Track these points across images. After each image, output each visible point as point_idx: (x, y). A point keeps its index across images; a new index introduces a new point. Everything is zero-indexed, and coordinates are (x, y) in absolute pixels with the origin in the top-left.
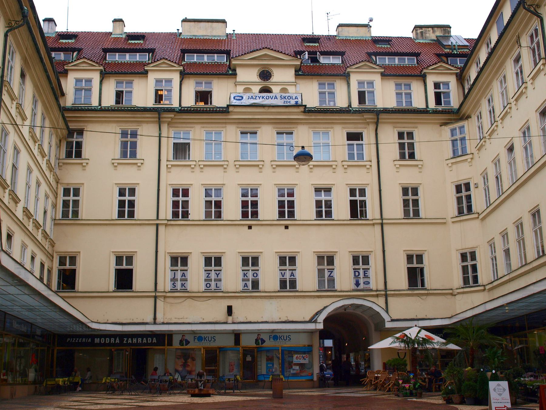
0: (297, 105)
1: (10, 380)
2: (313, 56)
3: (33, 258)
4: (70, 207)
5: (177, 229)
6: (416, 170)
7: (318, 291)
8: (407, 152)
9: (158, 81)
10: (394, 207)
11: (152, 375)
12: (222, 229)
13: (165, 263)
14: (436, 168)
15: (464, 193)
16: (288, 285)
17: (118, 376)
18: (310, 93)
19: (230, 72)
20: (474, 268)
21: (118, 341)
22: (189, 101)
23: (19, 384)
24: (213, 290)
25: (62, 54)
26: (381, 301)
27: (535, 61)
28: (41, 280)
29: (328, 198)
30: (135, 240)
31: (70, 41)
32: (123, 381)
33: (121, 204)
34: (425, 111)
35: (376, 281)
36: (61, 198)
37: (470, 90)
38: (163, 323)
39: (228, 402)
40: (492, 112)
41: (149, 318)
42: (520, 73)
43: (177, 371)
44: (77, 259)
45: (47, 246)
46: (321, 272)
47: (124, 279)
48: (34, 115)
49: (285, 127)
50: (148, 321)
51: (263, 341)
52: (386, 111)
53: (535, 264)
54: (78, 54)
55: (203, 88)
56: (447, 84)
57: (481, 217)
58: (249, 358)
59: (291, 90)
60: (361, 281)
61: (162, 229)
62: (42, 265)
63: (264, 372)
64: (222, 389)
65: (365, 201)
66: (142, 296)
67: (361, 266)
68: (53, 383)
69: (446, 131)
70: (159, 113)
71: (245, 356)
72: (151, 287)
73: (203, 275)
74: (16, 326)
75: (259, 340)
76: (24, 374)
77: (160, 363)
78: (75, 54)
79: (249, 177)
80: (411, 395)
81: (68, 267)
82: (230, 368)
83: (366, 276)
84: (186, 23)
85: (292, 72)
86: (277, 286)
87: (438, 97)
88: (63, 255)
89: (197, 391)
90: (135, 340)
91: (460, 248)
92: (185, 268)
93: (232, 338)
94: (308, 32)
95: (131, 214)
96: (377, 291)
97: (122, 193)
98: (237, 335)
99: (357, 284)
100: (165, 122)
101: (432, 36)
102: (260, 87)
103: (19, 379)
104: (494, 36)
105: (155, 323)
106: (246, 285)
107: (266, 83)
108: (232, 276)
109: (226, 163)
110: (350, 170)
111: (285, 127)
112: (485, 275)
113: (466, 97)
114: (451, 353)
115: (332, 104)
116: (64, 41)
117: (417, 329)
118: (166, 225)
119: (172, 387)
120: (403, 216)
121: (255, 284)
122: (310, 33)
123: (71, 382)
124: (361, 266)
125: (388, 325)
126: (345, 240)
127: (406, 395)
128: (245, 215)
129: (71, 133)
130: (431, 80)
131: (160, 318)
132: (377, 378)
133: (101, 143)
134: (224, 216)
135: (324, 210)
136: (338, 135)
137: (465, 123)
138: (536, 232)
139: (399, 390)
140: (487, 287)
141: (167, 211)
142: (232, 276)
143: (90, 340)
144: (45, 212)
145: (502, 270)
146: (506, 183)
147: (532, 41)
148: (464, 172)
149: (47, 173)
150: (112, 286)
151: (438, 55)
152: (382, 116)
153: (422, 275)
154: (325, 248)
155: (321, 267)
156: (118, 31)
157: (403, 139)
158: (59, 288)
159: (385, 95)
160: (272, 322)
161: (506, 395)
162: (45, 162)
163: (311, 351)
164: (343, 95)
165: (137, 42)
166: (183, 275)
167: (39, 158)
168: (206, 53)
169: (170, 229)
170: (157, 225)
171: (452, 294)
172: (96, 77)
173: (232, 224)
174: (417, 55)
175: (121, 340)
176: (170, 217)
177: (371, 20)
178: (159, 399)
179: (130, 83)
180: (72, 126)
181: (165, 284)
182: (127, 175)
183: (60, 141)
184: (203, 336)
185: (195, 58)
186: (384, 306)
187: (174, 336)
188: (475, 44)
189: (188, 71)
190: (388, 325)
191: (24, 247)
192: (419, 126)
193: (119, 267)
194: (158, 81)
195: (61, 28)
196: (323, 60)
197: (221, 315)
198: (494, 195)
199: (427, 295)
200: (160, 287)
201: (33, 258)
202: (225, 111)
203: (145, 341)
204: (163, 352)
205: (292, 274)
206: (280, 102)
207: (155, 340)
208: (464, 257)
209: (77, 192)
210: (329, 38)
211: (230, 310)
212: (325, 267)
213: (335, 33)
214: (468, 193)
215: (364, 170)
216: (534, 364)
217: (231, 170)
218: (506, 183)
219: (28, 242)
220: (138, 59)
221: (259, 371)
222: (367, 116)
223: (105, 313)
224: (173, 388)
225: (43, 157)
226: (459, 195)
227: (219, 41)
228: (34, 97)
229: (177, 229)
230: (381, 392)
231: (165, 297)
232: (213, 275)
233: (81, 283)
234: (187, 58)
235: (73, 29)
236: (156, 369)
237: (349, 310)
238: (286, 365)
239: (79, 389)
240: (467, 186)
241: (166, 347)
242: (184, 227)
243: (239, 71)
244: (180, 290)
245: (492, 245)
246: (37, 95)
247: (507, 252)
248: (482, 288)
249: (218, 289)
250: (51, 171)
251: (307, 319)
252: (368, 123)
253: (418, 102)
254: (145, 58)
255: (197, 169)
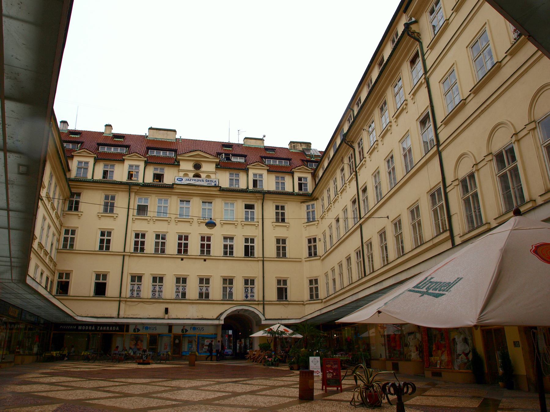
0: (215, 186)
1: (21, 352)
2: (229, 156)
3: (42, 274)
4: (68, 241)
5: (136, 259)
6: (285, 229)
7: (222, 300)
8: (281, 218)
9: (131, 166)
10: (271, 250)
11: (115, 350)
12: (165, 260)
13: (127, 280)
14: (297, 229)
15: (312, 244)
16: (204, 296)
17: (92, 351)
18: (224, 179)
19: (175, 164)
20: (317, 288)
21: (93, 328)
22: (149, 179)
23: (27, 355)
24: (157, 297)
25: (71, 145)
26: (260, 308)
27: (351, 172)
28: (46, 288)
29: (231, 243)
30: (110, 265)
31: (76, 136)
32: (95, 354)
33: (102, 241)
34: (292, 194)
35: (258, 296)
36: (63, 235)
37: (319, 181)
38: (124, 318)
39: (3, 40)
40: (329, 197)
41: (115, 314)
42: (343, 177)
43: (130, 348)
44: (71, 275)
45: (51, 266)
46: (225, 289)
47: (100, 289)
48: (50, 184)
49: (207, 199)
50: (114, 316)
51: (187, 331)
52: (269, 192)
53: (347, 289)
54: (81, 145)
55: (158, 172)
56: (306, 178)
57: (322, 258)
58: (177, 341)
59: (213, 176)
60: (249, 295)
61: (126, 258)
62: (47, 278)
63: (186, 350)
64: (158, 360)
65: (254, 246)
66: (111, 299)
67: (249, 286)
68: (49, 354)
69: (304, 206)
70: (130, 186)
71: (175, 339)
72: (117, 295)
73: (151, 288)
74: (28, 317)
75: (184, 330)
76: (31, 349)
77: (120, 343)
78: (79, 145)
79: (184, 229)
80: (272, 365)
81: (64, 280)
82: (164, 347)
83: (252, 292)
84: (151, 130)
85: (214, 165)
86: (197, 296)
87: (300, 185)
88: (61, 272)
89: (141, 361)
90: (105, 328)
91: (309, 276)
92: (140, 283)
93: (168, 328)
94: (226, 140)
95: (108, 248)
96: (258, 301)
97: (103, 234)
98: (170, 327)
99: (247, 297)
100: (133, 191)
101: (300, 148)
102: (194, 173)
103: (27, 352)
104: (332, 153)
105: (118, 318)
106: (178, 295)
107: (198, 172)
108: (169, 289)
109: (170, 218)
110: (245, 227)
111: (207, 199)
112: (322, 294)
113: (316, 185)
114: (297, 340)
115: (237, 186)
116: (73, 136)
117: (278, 325)
118: (129, 256)
119: (127, 358)
120: (276, 256)
121: (184, 295)
122: (227, 141)
123: (61, 355)
124: (249, 286)
125: (263, 322)
126: (240, 270)
127: (269, 365)
128: (179, 251)
129: (72, 194)
130: (297, 176)
131: (122, 314)
132: (254, 354)
133: (91, 201)
134: (167, 252)
135: (228, 251)
136: (239, 206)
137: (315, 202)
138: (348, 270)
139: (265, 362)
140: (324, 301)
141: (130, 247)
142: (169, 289)
143: (75, 327)
144: (52, 244)
145: (331, 291)
146: (335, 240)
147: (350, 161)
148: (313, 231)
149: (55, 220)
150: (92, 293)
151: (303, 160)
152: (266, 195)
153: (286, 292)
154: (228, 274)
155: (225, 286)
156: (108, 132)
157: (279, 210)
158: (57, 293)
159: (269, 183)
160: (193, 319)
161: (319, 365)
162: (54, 213)
163: (216, 337)
164: (244, 182)
165: (120, 141)
166: (139, 288)
167: (51, 211)
168: (161, 149)
169: (132, 258)
170: (124, 256)
171: (303, 304)
172: (91, 161)
173: (171, 257)
174: (290, 160)
175: (96, 328)
176: (132, 251)
177: (264, 136)
178: (117, 365)
179: (113, 166)
180: (74, 190)
181: (127, 293)
182: (107, 224)
183: (65, 200)
184: (149, 326)
185: (155, 153)
186: (261, 310)
187: (130, 326)
188: (324, 154)
189: (149, 161)
190: (263, 322)
191: (37, 267)
192: (289, 203)
193: (97, 281)
194: (131, 166)
195: (71, 127)
196: (234, 159)
197: (519, 349)
198: (328, 247)
199: (288, 304)
200: (123, 295)
201: (42, 274)
202: (171, 187)
203: (111, 328)
204: (123, 336)
205: (207, 290)
206: (205, 184)
207: (117, 329)
208: (311, 282)
209: (73, 232)
210: (239, 145)
211: (167, 311)
212: (228, 285)
213: (242, 143)
214: (315, 244)
215: (254, 227)
216: (345, 348)
217: (173, 223)
218: (335, 240)
219: (40, 264)
220: (119, 151)
221: (183, 349)
222: (257, 195)
223: (85, 310)
224: (127, 359)
225: (54, 210)
226: (310, 245)
227: (171, 143)
228: (51, 173)
229: (136, 259)
230: (256, 363)
231: (126, 301)
232: (157, 288)
233: (72, 290)
234: (150, 153)
235: (79, 128)
236: (117, 347)
237: (241, 313)
238: (200, 346)
239: (66, 359)
240: (315, 240)
241: (125, 333)
242: (141, 258)
243: (181, 163)
244: (136, 297)
245: (326, 275)
246: (53, 172)
247: (334, 280)
248: (320, 301)
249: (160, 297)
250: (58, 219)
251: (215, 317)
252: (258, 199)
253: (288, 188)
254: (124, 151)
255: (151, 222)
